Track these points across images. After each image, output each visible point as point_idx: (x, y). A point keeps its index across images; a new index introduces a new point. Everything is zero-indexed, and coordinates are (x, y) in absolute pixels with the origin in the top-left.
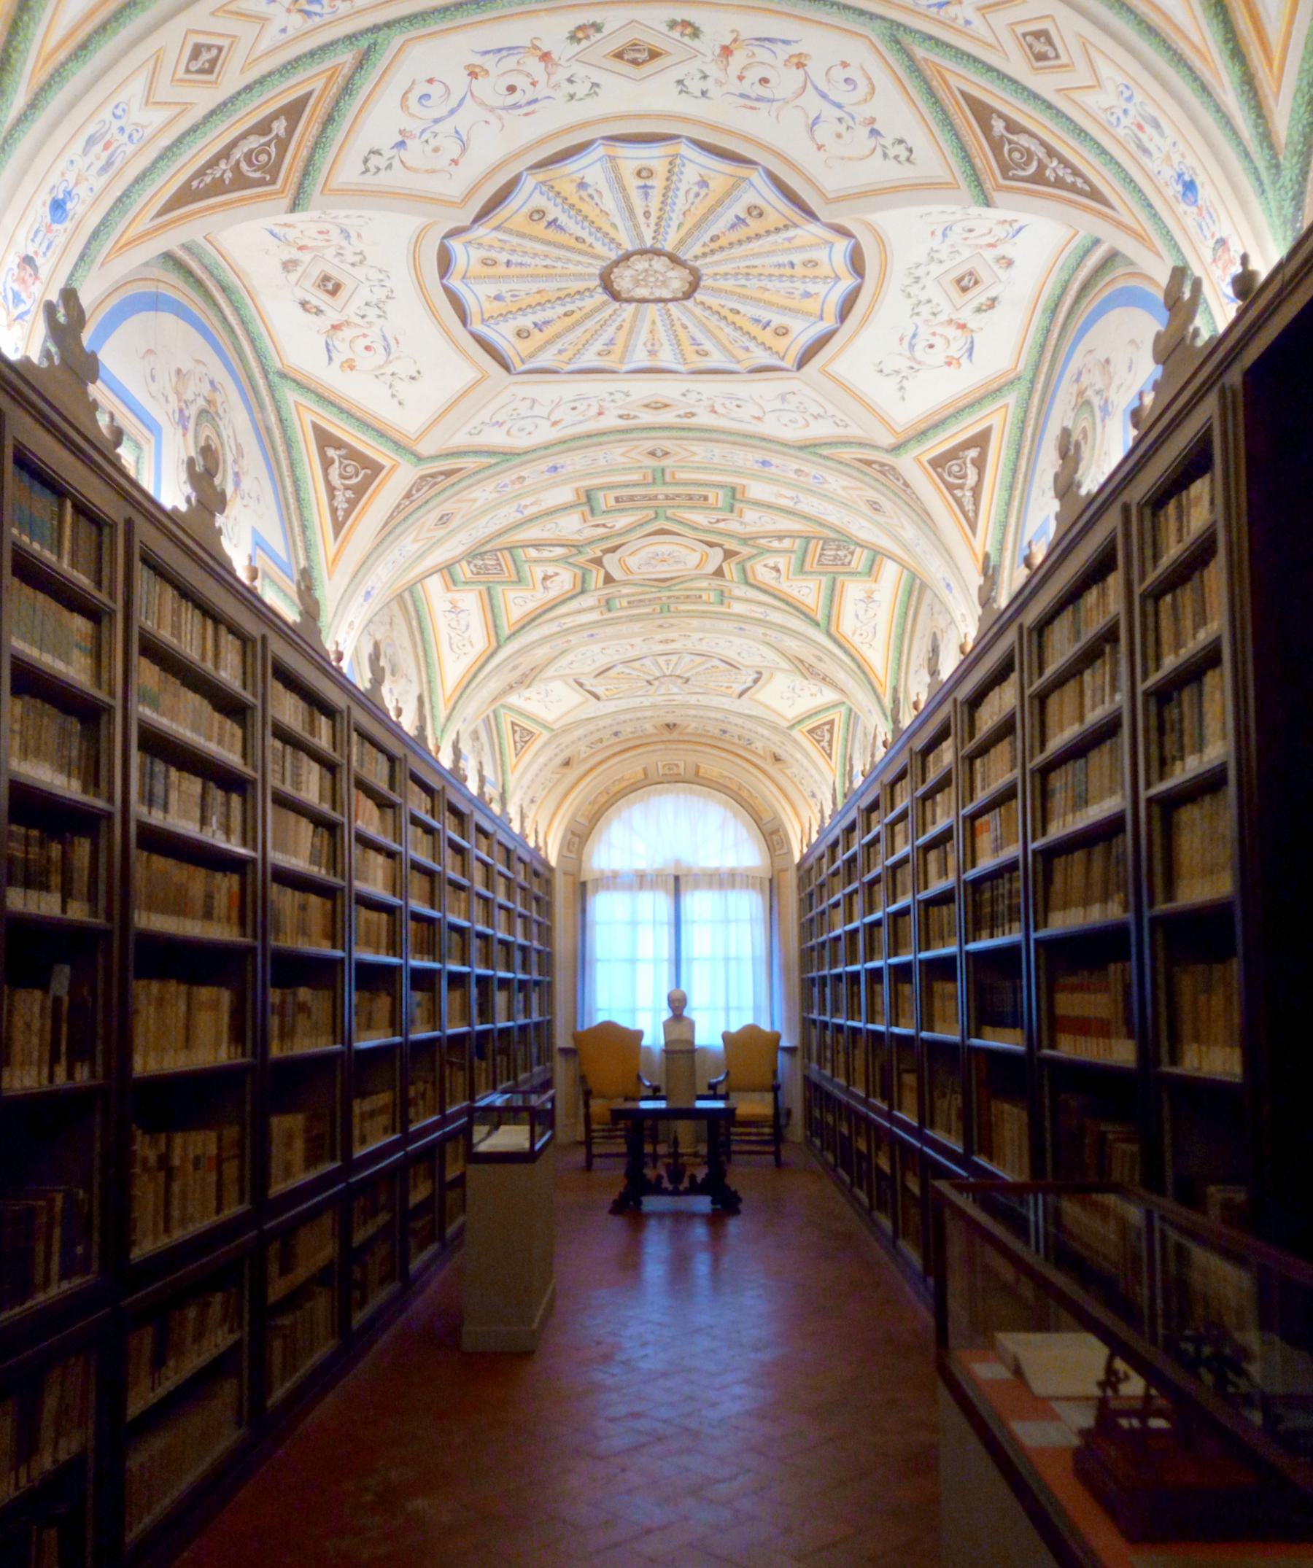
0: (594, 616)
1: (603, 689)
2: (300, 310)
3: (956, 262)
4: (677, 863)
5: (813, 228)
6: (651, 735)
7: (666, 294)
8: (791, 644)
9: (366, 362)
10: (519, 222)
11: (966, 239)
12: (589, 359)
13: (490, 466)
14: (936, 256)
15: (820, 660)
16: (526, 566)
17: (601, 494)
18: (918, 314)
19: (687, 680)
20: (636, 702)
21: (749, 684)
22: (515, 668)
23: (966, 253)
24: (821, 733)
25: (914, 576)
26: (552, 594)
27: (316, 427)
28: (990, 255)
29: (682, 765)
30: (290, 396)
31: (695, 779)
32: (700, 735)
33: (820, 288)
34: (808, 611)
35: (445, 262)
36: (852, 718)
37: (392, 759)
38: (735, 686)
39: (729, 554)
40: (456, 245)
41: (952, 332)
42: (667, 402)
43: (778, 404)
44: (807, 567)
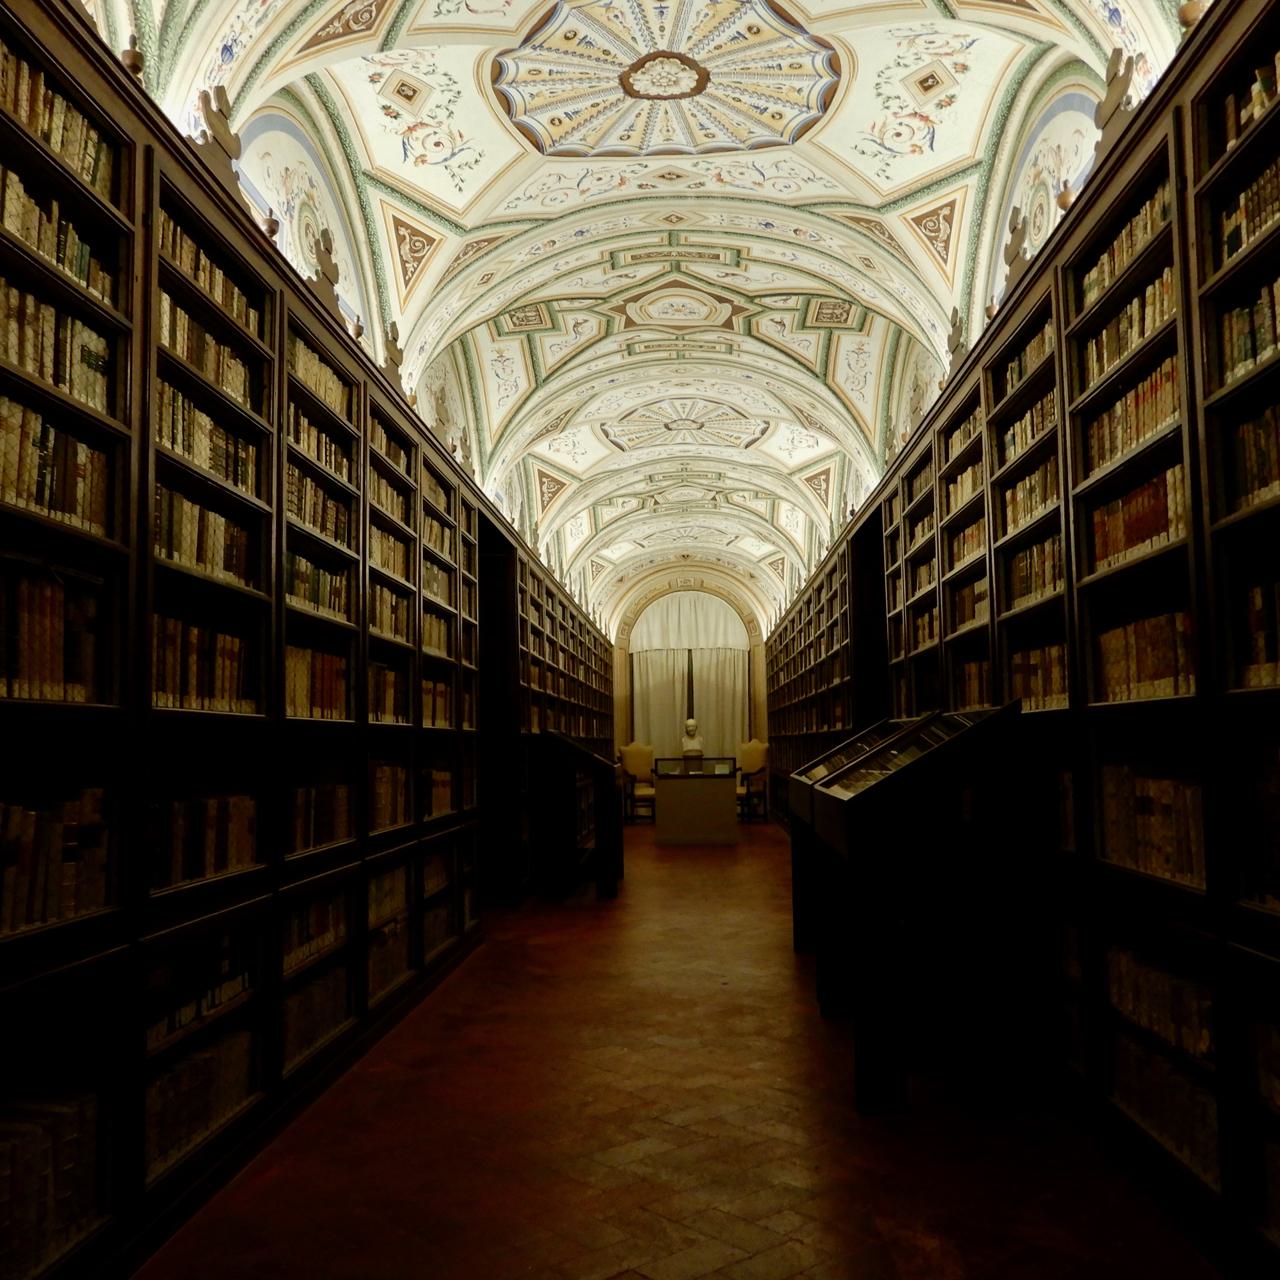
0: (617, 360)
1: (625, 439)
2: (382, 113)
3: (918, 67)
5: (800, 38)
6: (673, 562)
7: (676, 91)
8: (790, 393)
9: (563, 449)
10: (557, 41)
11: (927, 49)
12: (612, 142)
13: (526, 232)
14: (902, 62)
15: (814, 407)
16: (560, 315)
17: (622, 255)
18: (887, 108)
19: (702, 426)
21: (757, 435)
22: (547, 413)
23: (927, 59)
24: (777, 565)
26: (583, 339)
27: (394, 217)
28: (948, 62)
29: (692, 580)
30: (374, 196)
32: (704, 562)
33: (805, 84)
34: (809, 365)
35: (498, 72)
36: (846, 465)
38: (743, 436)
39: (737, 310)
40: (507, 60)
41: (916, 123)
42: (680, 173)
44: (808, 324)
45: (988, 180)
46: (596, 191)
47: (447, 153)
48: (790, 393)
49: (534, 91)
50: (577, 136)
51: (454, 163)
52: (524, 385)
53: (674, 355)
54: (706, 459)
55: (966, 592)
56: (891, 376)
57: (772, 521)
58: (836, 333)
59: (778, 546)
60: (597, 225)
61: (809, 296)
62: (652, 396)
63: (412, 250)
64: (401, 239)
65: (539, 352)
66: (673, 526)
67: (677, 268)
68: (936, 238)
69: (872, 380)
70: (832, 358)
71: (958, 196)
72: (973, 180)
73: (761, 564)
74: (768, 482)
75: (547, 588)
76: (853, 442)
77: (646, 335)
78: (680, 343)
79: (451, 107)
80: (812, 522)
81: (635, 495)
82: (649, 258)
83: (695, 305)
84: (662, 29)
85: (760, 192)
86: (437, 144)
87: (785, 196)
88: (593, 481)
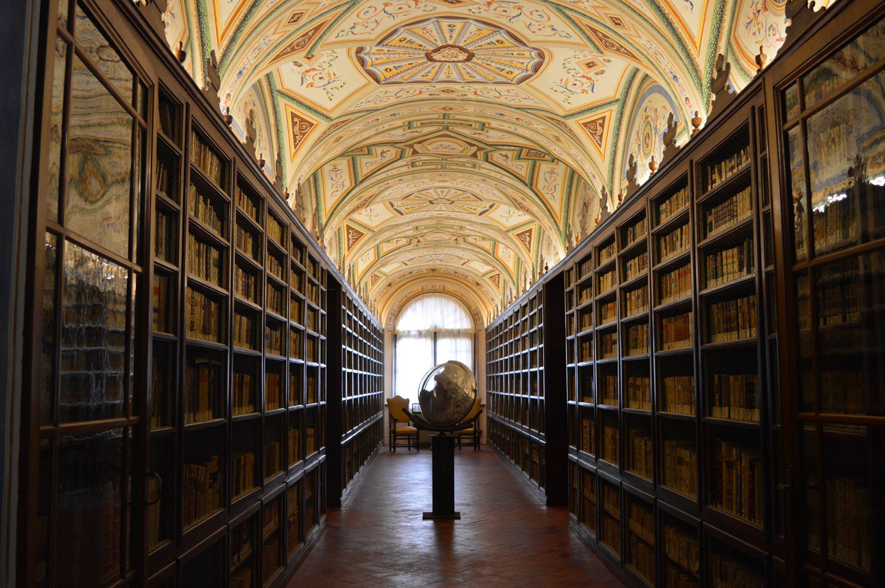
1: (404, 208)
4: (435, 327)
7: (455, 59)
8: (510, 191)
12: (418, 77)
19: (453, 202)
20: (420, 215)
21: (487, 208)
22: (360, 198)
24: (495, 279)
25: (573, 172)
26: (386, 160)
30: (281, 101)
31: (442, 292)
33: (526, 61)
37: (281, 224)
38: (479, 209)
39: (479, 149)
41: (584, 80)
43: (506, 93)
44: (522, 156)
45: (623, 108)
46: (404, 96)
47: (325, 82)
48: (510, 191)
49: (378, 57)
50: (399, 76)
51: (328, 87)
52: (347, 185)
53: (440, 167)
54: (453, 219)
55: (608, 337)
56: (570, 193)
57: (494, 254)
58: (538, 162)
59: (532, 214)
60: (404, 111)
61: (522, 148)
62: (423, 187)
63: (300, 129)
64: (294, 124)
65: (358, 166)
66: (430, 185)
67: (447, 129)
68: (595, 134)
69: (559, 188)
70: (536, 175)
71: (607, 114)
72: (615, 108)
73: (484, 278)
74: (492, 233)
75: (293, 235)
76: (547, 222)
77: (423, 158)
78: (444, 162)
79: (331, 63)
80: (519, 259)
81: (393, 144)
82: (431, 124)
83: (455, 146)
84: (451, 37)
85: (498, 100)
86: (321, 78)
87: (512, 103)
88: (381, 232)
